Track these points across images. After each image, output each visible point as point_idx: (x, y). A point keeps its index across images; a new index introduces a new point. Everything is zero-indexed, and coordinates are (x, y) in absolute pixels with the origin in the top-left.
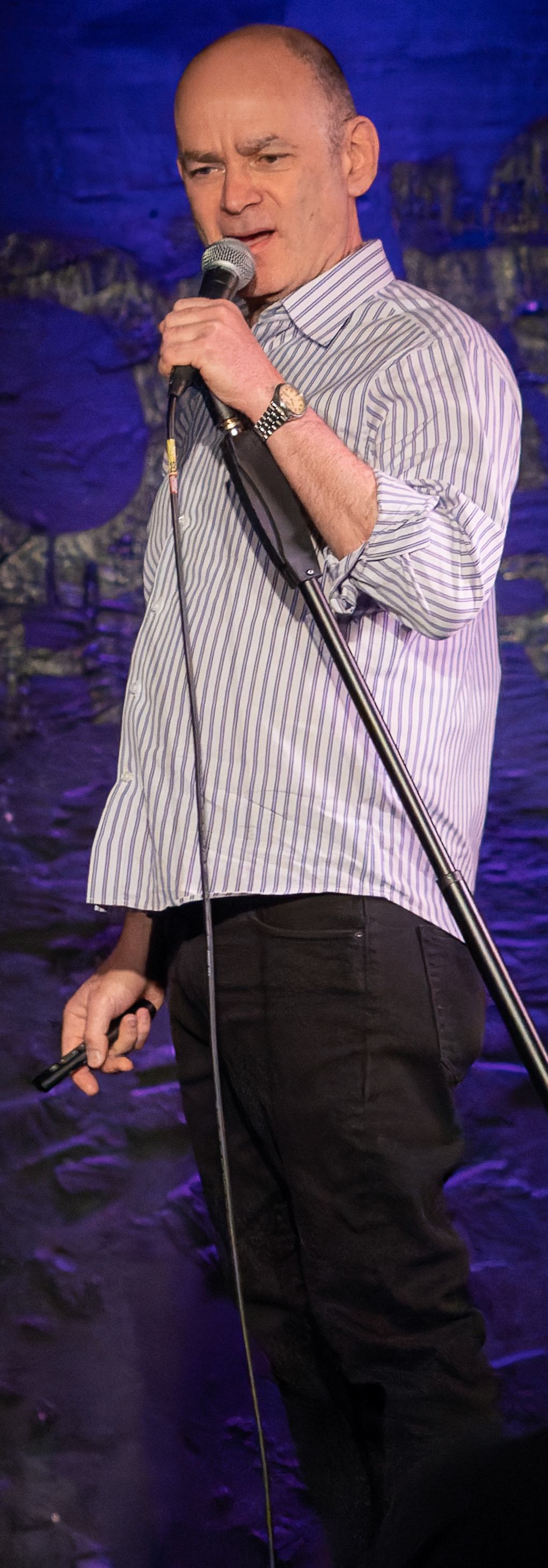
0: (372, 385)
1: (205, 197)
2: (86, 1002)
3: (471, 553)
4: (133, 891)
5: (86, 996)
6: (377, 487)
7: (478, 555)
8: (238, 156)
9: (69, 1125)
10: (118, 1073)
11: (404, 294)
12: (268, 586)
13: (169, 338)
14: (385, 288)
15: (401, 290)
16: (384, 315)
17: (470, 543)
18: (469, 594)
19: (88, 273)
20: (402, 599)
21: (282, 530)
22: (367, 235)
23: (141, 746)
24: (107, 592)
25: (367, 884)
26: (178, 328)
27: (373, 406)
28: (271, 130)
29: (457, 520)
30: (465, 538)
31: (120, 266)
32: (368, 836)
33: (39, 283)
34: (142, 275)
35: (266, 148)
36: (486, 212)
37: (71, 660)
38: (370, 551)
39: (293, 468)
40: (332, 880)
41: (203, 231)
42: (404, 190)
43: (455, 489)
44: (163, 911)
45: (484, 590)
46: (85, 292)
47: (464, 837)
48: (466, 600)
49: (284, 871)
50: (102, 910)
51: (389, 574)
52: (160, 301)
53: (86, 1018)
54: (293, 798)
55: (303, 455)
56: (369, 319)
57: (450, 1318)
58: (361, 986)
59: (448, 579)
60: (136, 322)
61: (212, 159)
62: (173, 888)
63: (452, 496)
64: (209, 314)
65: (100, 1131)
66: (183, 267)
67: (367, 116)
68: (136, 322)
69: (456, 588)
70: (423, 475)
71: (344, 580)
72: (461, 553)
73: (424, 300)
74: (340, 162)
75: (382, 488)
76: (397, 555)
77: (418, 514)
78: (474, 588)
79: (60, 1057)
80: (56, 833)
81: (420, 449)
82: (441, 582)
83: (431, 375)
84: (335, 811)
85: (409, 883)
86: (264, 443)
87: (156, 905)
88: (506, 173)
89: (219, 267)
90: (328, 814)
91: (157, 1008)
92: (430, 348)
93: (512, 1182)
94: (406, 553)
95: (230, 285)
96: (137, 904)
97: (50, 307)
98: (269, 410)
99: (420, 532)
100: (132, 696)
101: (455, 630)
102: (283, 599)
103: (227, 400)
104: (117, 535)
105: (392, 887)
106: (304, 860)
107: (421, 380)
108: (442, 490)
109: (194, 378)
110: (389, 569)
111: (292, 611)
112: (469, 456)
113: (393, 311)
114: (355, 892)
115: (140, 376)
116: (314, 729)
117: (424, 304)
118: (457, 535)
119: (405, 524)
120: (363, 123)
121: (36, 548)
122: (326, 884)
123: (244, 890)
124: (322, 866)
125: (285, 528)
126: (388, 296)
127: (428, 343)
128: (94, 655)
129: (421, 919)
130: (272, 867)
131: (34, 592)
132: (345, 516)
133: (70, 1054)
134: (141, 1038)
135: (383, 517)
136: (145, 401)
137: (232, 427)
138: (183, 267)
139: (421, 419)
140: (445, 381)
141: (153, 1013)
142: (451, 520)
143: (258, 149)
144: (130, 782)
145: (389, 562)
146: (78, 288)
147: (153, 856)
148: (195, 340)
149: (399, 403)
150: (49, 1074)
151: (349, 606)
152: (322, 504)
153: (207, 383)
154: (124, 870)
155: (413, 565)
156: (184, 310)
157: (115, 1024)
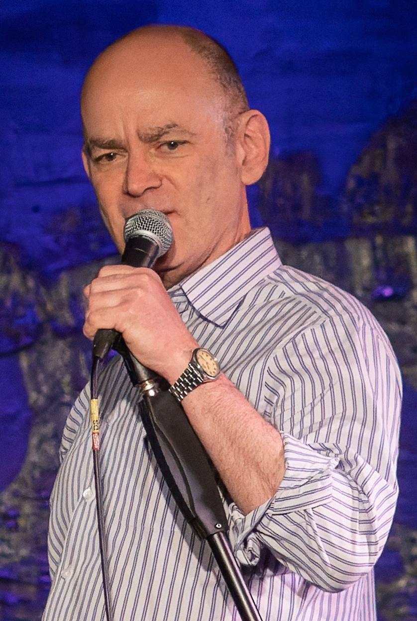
0: (271, 363)
1: (109, 184)
3: (367, 511)
6: (284, 446)
7: (375, 513)
8: (140, 143)
11: (292, 277)
12: (186, 547)
13: (95, 303)
14: (275, 272)
16: (275, 297)
17: (368, 501)
18: (365, 549)
22: (256, 224)
26: (104, 293)
27: (272, 382)
28: (171, 122)
30: (363, 497)
34: (27, 266)
35: (166, 135)
38: (276, 505)
43: (353, 451)
45: (379, 546)
48: (362, 555)
52: (42, 290)
56: (260, 301)
59: (348, 535)
61: (116, 148)
63: (351, 458)
64: (133, 281)
66: (93, 244)
68: (21, 311)
69: (354, 542)
70: (322, 439)
71: (249, 534)
72: (361, 511)
73: (311, 283)
74: (234, 153)
75: (288, 447)
76: (301, 510)
77: (321, 472)
78: (370, 544)
83: (325, 351)
88: (361, 170)
92: (323, 326)
94: (309, 508)
95: (151, 254)
98: (183, 376)
99: (323, 489)
101: (351, 582)
102: (191, 548)
103: (147, 362)
107: (316, 355)
108: (341, 453)
109: (118, 342)
110: (293, 522)
111: (200, 559)
112: (364, 424)
113: (283, 293)
115: (24, 361)
118: (356, 494)
119: (310, 481)
125: (195, 480)
127: (320, 322)
132: (254, 474)
135: (290, 474)
136: (29, 385)
137: (150, 388)
138: (93, 244)
139: (319, 391)
140: (338, 355)
142: (350, 481)
143: (159, 136)
145: (293, 516)
148: (121, 304)
149: (296, 378)
151: (253, 557)
152: (232, 460)
153: (128, 346)
155: (316, 520)
156: (109, 277)
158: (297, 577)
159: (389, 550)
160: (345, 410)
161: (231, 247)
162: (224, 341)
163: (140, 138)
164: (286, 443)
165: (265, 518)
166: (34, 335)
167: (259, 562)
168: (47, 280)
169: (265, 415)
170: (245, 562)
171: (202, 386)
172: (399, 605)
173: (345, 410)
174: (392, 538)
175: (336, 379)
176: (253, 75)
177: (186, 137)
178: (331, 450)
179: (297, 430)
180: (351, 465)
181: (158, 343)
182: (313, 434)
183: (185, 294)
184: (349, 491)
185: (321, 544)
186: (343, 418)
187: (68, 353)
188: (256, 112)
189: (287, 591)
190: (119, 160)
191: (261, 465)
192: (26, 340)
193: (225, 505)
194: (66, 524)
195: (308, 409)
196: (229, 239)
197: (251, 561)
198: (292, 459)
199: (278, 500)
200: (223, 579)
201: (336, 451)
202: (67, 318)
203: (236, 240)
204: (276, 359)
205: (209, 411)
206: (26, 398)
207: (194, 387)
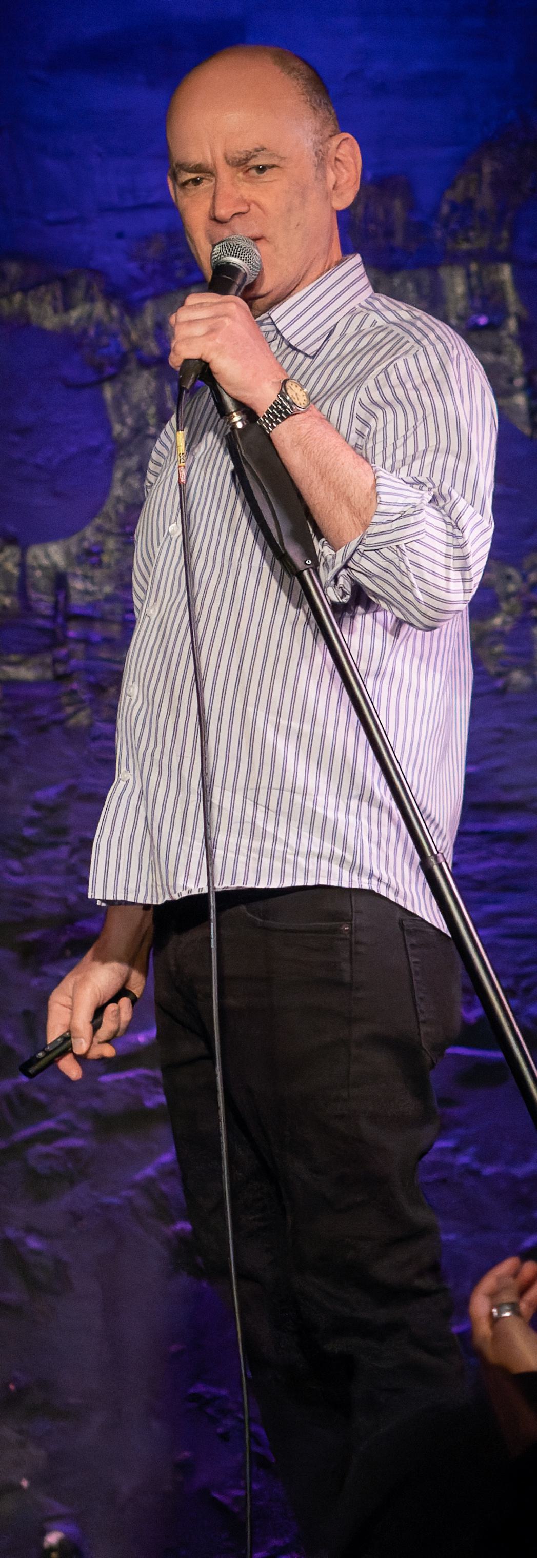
0: (362, 394)
1: (195, 210)
4: (132, 886)
7: (469, 549)
9: (40, 1110)
10: (102, 1059)
11: (384, 306)
12: (274, 584)
13: (181, 332)
14: (366, 300)
16: (366, 326)
17: (462, 537)
18: (460, 586)
19: (59, 294)
20: (397, 590)
21: (280, 526)
22: (347, 250)
23: (139, 746)
24: (77, 601)
25: (355, 877)
26: (190, 322)
27: (363, 414)
28: (257, 143)
30: (457, 532)
31: (89, 287)
32: (357, 830)
34: (112, 294)
35: (254, 159)
37: (42, 664)
38: (368, 541)
39: (295, 460)
40: (324, 873)
41: (193, 241)
43: (447, 485)
45: (473, 583)
46: (56, 311)
48: (456, 592)
49: (277, 864)
50: (104, 905)
52: (127, 319)
54: (287, 795)
55: (305, 447)
56: (351, 331)
58: (347, 978)
59: (442, 571)
60: (105, 340)
61: (203, 172)
62: (171, 883)
63: (445, 492)
64: (220, 309)
65: (66, 1115)
66: (178, 271)
67: (349, 132)
68: (105, 340)
69: (448, 579)
70: (415, 473)
71: (340, 570)
72: (455, 547)
73: (404, 311)
74: (325, 177)
75: (380, 481)
76: (394, 545)
77: (414, 507)
78: (464, 580)
79: (47, 1046)
80: (28, 832)
82: (434, 573)
83: (418, 381)
84: (326, 807)
87: (155, 899)
88: (455, 195)
89: (228, 263)
90: (320, 810)
92: (415, 356)
93: (463, 1159)
94: (401, 544)
95: (238, 282)
96: (136, 898)
98: (272, 408)
99: (415, 524)
100: (128, 698)
101: (445, 620)
102: (280, 585)
103: (234, 393)
104: (86, 544)
105: (380, 880)
106: (297, 854)
107: (409, 385)
108: (434, 487)
109: (204, 372)
110: (385, 558)
111: (289, 597)
112: (458, 457)
113: (375, 322)
114: (345, 885)
115: (108, 392)
116: (307, 728)
117: (405, 316)
118: (450, 529)
119: (403, 515)
121: (8, 560)
122: (318, 876)
123: (239, 884)
125: (284, 514)
126: (370, 308)
127: (413, 352)
129: (405, 910)
130: (266, 861)
131: (7, 601)
133: (56, 1041)
134: (123, 1025)
135: (382, 508)
136: (113, 417)
137: (238, 421)
138: (178, 271)
139: (411, 423)
140: (432, 386)
141: (134, 1001)
143: (247, 159)
144: (128, 782)
145: (385, 552)
147: (151, 851)
148: (207, 334)
149: (388, 410)
151: (344, 594)
153: (216, 376)
154: (136, 855)
155: (409, 556)
156: (195, 305)
157: (99, 1012)
158: (389, 615)
160: (438, 443)
161: (321, 275)
162: (314, 371)
163: (228, 162)
164: (378, 477)
165: (356, 554)
166: (117, 366)
167: (350, 600)
168: (132, 309)
169: (356, 447)
170: (335, 599)
171: (291, 418)
172: (494, 643)
173: (438, 443)
174: (488, 575)
175: (429, 410)
176: (343, 97)
177: (275, 161)
178: (424, 484)
179: (389, 463)
181: (247, 375)
182: (406, 467)
183: (273, 323)
186: (437, 451)
187: (153, 384)
188: (347, 135)
189: (379, 629)
190: (206, 185)
191: (352, 499)
192: (109, 370)
193: (315, 541)
194: (151, 561)
195: (400, 442)
196: (319, 266)
198: (384, 493)
199: (369, 536)
200: (312, 617)
201: (430, 485)
202: (152, 347)
204: (367, 390)
205: (299, 444)
206: (110, 430)
207: (283, 419)
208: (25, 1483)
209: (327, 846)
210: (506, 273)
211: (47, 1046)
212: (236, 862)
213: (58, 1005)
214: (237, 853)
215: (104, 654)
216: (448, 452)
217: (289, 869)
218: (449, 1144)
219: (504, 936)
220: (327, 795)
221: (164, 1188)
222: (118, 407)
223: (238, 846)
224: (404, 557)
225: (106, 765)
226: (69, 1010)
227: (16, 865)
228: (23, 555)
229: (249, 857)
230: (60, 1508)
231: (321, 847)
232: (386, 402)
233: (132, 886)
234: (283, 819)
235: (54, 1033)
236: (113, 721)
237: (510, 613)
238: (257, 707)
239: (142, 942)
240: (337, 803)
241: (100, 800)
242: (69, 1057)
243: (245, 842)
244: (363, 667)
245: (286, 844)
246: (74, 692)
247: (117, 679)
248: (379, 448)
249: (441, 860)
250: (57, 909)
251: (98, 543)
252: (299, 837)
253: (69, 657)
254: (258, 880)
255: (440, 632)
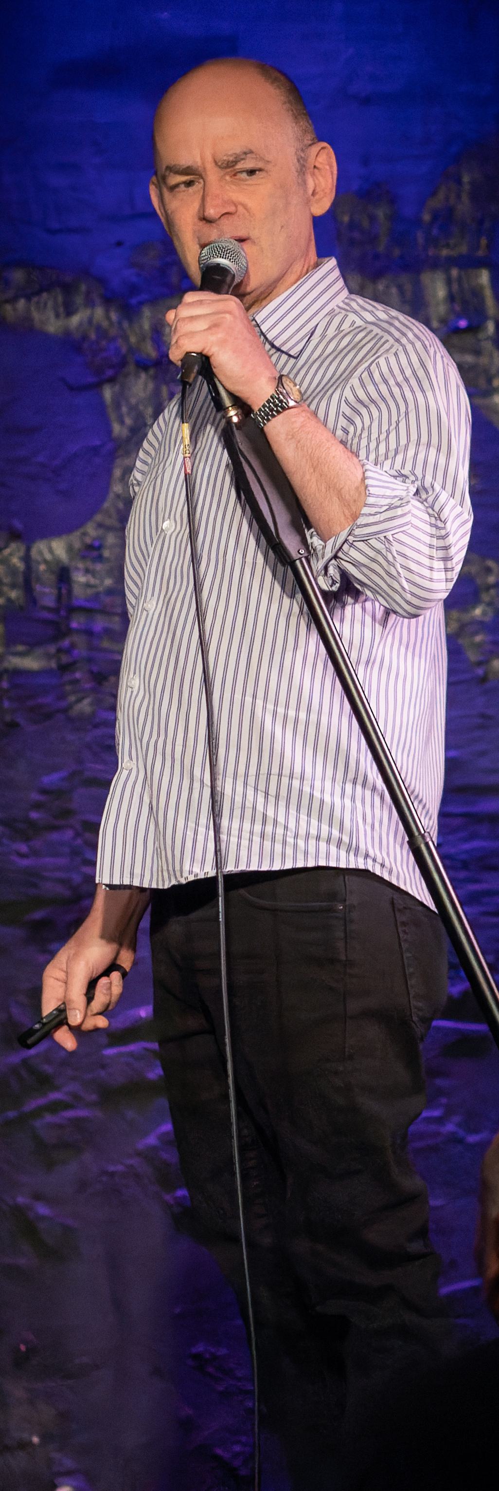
0: (348, 393)
1: (183, 212)
2: (64, 966)
3: (443, 538)
4: (138, 871)
5: (65, 961)
6: (364, 473)
7: (451, 539)
8: (217, 169)
9: (44, 1082)
10: (97, 1030)
12: (269, 575)
13: (185, 328)
15: (357, 303)
16: (346, 326)
17: (444, 528)
18: (442, 575)
19: (60, 299)
22: (323, 253)
24: (78, 592)
26: (192, 318)
28: (242, 155)
29: (432, 508)
31: (88, 294)
33: (15, 310)
34: (108, 300)
36: (420, 237)
37: (49, 657)
38: (357, 532)
39: (288, 452)
40: (323, 854)
42: (346, 219)
44: (168, 889)
45: (454, 572)
46: (57, 316)
47: (430, 812)
48: (439, 581)
49: (278, 847)
51: (372, 554)
52: (126, 325)
53: (66, 983)
56: (331, 332)
57: (411, 1258)
59: (426, 561)
61: (193, 175)
62: (177, 868)
63: (427, 484)
64: (220, 306)
65: (73, 1087)
66: (170, 280)
68: (104, 343)
69: (431, 569)
70: (398, 466)
73: (381, 312)
74: (305, 182)
75: (368, 474)
76: (381, 536)
77: (401, 499)
78: (446, 570)
79: (42, 1019)
80: (34, 815)
81: (393, 446)
82: (419, 563)
83: (400, 378)
84: (322, 791)
85: (388, 854)
86: (262, 430)
88: (436, 202)
89: (219, 264)
90: (317, 794)
91: (128, 970)
92: (396, 354)
93: (450, 1127)
94: (389, 535)
97: (27, 331)
102: (274, 575)
104: (88, 540)
105: (374, 860)
106: (296, 836)
107: (392, 382)
108: (417, 479)
109: (204, 365)
110: (372, 548)
111: (283, 588)
112: (439, 450)
113: (354, 322)
114: (343, 865)
115: (108, 393)
117: (382, 316)
118: (433, 521)
119: (391, 508)
120: (323, 148)
121: (14, 554)
123: (242, 867)
124: (312, 842)
125: (276, 506)
127: (393, 350)
128: (69, 651)
131: (13, 594)
132: (335, 499)
133: (51, 1014)
134: (114, 999)
135: (371, 500)
136: (113, 416)
137: (234, 415)
139: (394, 418)
140: (413, 382)
141: (124, 975)
143: (236, 162)
145: (373, 542)
146: (51, 314)
148: (209, 328)
150: (32, 1032)
153: (214, 370)
154: (144, 838)
155: (395, 547)
157: (92, 985)
158: (377, 604)
159: (464, 580)
160: (419, 437)
164: (366, 470)
167: (339, 588)
168: (130, 312)
169: (342, 442)
170: (325, 587)
171: (287, 412)
172: (476, 633)
173: (419, 437)
175: (411, 406)
176: (321, 111)
177: (260, 165)
179: (372, 457)
180: (427, 492)
181: (243, 372)
182: (389, 461)
183: (258, 326)
184: (427, 517)
185: (400, 570)
187: (151, 386)
188: (325, 144)
189: (368, 620)
190: (198, 187)
192: (110, 373)
194: (145, 560)
196: (298, 268)
197: (331, 586)
198: (372, 486)
199: (358, 527)
201: (412, 478)
202: (150, 351)
203: (305, 269)
204: (352, 388)
205: (293, 437)
206: (109, 431)
207: (278, 412)
208: (36, 1440)
209: (325, 828)
210: (484, 277)
211: (42, 1019)
212: (239, 845)
213: (52, 980)
214: (240, 837)
215: (106, 644)
216: (429, 444)
217: (289, 851)
218: (436, 1113)
219: (485, 914)
220: (323, 779)
221: (165, 1156)
222: (117, 405)
223: (240, 830)
224: (391, 548)
225: (106, 753)
226: (63, 984)
227: (24, 848)
228: (28, 549)
229: (251, 841)
230: (69, 1463)
231: (319, 829)
232: (369, 401)
233: (138, 871)
234: (282, 804)
235: (49, 1006)
236: (113, 708)
237: (489, 604)
238: (254, 697)
239: (130, 919)
240: (333, 787)
241: (105, 785)
242: (65, 1028)
243: (247, 826)
244: (354, 656)
245: (286, 828)
246: (77, 681)
247: (114, 669)
248: (364, 443)
249: (428, 839)
250: (61, 891)
251: (101, 538)
252: (298, 821)
253: (73, 646)
254: (260, 863)
255: (425, 618)
